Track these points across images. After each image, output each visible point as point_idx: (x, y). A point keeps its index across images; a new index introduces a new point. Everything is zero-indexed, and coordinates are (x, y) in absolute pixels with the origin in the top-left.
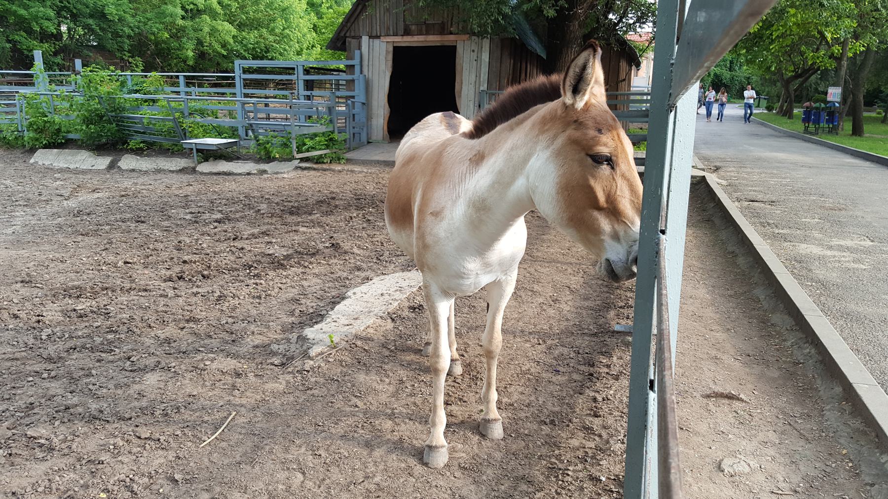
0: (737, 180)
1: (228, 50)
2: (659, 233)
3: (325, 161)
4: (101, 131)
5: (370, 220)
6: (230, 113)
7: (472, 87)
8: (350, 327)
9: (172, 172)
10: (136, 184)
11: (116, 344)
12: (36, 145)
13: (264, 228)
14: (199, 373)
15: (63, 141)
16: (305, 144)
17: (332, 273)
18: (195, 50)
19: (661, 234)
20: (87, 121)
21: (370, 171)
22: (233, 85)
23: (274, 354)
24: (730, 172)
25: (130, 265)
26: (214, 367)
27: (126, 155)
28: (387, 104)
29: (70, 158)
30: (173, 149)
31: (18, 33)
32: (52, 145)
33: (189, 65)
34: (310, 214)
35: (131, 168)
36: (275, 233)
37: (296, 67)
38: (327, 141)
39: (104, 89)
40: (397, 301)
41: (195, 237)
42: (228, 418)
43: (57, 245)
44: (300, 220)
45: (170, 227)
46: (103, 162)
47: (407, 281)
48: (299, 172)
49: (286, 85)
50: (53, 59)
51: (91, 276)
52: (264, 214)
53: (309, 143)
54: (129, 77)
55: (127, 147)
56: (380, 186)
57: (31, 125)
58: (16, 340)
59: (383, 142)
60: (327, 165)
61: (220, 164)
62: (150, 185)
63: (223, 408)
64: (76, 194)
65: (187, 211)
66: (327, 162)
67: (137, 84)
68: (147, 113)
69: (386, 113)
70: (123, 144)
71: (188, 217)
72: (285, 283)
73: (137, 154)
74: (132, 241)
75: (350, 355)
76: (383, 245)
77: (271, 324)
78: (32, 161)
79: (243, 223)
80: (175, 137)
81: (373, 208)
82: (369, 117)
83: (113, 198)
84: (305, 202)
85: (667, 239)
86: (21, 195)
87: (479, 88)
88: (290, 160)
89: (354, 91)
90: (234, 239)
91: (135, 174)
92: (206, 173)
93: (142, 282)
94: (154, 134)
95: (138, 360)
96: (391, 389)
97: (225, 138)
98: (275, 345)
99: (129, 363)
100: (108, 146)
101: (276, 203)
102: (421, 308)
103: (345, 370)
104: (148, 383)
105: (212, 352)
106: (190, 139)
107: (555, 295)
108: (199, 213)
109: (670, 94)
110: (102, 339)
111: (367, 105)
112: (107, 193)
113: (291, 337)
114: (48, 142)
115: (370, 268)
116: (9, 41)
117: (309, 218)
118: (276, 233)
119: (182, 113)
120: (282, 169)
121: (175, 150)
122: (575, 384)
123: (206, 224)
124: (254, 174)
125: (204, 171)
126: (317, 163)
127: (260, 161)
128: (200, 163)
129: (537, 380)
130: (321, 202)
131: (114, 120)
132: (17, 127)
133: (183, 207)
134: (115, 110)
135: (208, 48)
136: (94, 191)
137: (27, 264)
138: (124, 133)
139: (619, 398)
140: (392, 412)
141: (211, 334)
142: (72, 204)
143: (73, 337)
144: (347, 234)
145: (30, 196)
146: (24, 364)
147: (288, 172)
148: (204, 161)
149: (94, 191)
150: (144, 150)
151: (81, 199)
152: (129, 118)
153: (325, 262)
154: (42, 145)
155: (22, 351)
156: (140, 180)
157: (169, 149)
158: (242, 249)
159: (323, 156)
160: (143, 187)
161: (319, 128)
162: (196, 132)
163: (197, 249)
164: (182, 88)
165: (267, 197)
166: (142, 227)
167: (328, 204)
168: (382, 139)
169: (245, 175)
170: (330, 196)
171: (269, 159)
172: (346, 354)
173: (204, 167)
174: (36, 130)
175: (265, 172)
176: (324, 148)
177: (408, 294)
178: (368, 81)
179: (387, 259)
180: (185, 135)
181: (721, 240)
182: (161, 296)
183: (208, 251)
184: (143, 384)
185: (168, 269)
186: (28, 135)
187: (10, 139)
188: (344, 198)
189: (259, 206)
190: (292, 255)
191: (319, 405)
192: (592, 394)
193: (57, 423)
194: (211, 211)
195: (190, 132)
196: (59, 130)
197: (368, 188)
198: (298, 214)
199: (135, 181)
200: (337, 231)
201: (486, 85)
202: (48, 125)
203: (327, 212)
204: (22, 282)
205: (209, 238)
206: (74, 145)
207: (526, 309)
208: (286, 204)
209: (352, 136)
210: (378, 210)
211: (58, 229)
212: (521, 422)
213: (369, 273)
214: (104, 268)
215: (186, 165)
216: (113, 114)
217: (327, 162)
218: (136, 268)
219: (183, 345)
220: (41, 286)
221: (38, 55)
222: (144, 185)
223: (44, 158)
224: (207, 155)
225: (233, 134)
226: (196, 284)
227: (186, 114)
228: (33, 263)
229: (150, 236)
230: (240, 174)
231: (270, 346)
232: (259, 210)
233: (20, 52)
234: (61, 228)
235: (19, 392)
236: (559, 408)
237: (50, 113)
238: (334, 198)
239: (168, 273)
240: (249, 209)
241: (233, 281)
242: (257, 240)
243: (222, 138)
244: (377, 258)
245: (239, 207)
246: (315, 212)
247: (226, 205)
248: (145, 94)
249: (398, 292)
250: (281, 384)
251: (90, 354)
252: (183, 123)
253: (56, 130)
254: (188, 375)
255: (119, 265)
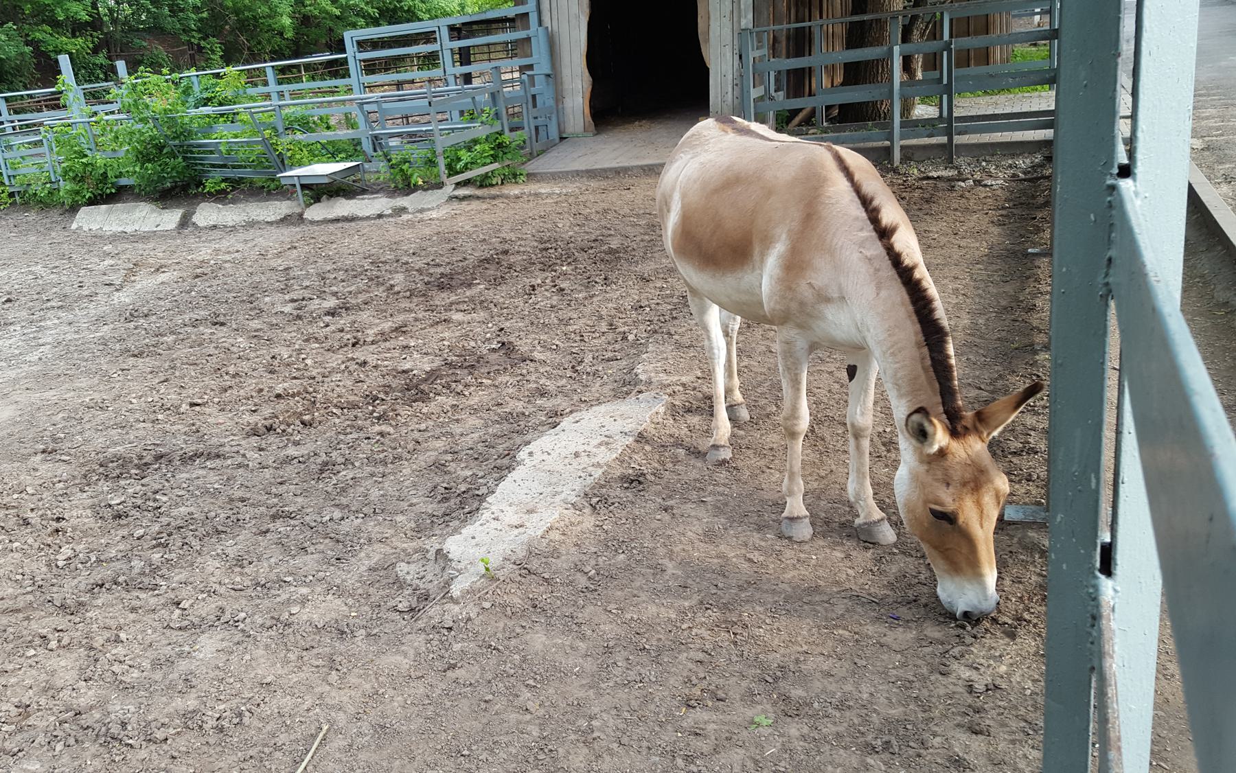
0: (1222, 135)
1: (341, 6)
2: (1098, 574)
3: (494, 182)
4: (163, 170)
5: (563, 290)
6: (347, 117)
7: (727, 22)
8: (521, 530)
9: (270, 223)
10: (217, 251)
11: (164, 571)
12: (77, 201)
13: (400, 319)
14: (281, 631)
15: (113, 191)
16: (459, 159)
17: (499, 404)
18: (294, 13)
19: (1102, 577)
20: (143, 157)
21: (564, 191)
22: (346, 74)
23: (399, 584)
24: (1207, 118)
25: (197, 408)
26: (305, 617)
27: (202, 205)
28: (587, 70)
29: (125, 216)
30: (269, 186)
31: (40, 28)
32: (99, 198)
33: (287, 39)
34: (470, 285)
35: (212, 223)
36: (415, 329)
37: (437, 29)
38: (493, 149)
39: (158, 104)
40: (602, 467)
41: (297, 347)
42: (317, 735)
43: (98, 377)
44: (453, 298)
45: (261, 329)
46: (170, 218)
47: (620, 422)
48: (456, 205)
49: (431, 60)
50: (93, 60)
51: (142, 433)
52: (399, 292)
53: (465, 156)
54: (194, 79)
55: (203, 190)
56: (580, 220)
57: (65, 172)
58: (21, 571)
59: (585, 134)
60: (497, 188)
61: (338, 204)
62: (237, 251)
63: (311, 714)
64: (133, 278)
65: (287, 297)
66: (497, 184)
67: (207, 89)
68: (224, 136)
69: (585, 86)
70: (198, 187)
71: (288, 309)
72: (424, 431)
73: (218, 201)
74: (204, 361)
75: (519, 593)
76: (583, 340)
77: (399, 518)
78: (74, 226)
79: (368, 313)
80: (270, 167)
81: (569, 264)
82: (559, 97)
83: (184, 281)
84: (460, 264)
85: (1118, 588)
86: (54, 290)
87: (739, 22)
88: (440, 186)
89: (532, 56)
90: (354, 345)
91: (216, 234)
92: (318, 221)
93: (214, 441)
94: (240, 167)
95: (192, 605)
96: (590, 665)
97: (342, 160)
98: (403, 564)
99: (178, 612)
100: (177, 190)
101: (417, 270)
102: (641, 479)
103: (510, 623)
104: (201, 656)
105: (305, 584)
106: (291, 169)
107: (888, 430)
108: (303, 299)
109: (1110, 260)
110: (143, 563)
111: (553, 77)
112: (175, 273)
113: (428, 547)
114: (93, 194)
115: (561, 391)
116: (27, 44)
117: (468, 293)
118: (416, 329)
119: (275, 129)
120: (429, 202)
121: (270, 190)
122: (930, 649)
123: (313, 320)
124: (389, 216)
125: (316, 219)
126: (481, 186)
127: (395, 192)
128: (308, 205)
129: (857, 641)
130: (487, 260)
131: (179, 152)
132: (49, 177)
133: (282, 291)
134: (178, 137)
135: (312, 8)
136: (158, 270)
137: (54, 417)
138: (195, 170)
139: (1019, 683)
140: (590, 725)
141: (305, 545)
142: (124, 298)
143: (102, 561)
144: (527, 321)
145: (68, 290)
146: (28, 619)
147: (438, 207)
148: (315, 202)
149: (158, 270)
150: (228, 193)
151: (139, 286)
152: (200, 146)
153: (490, 381)
154: (84, 200)
155: (28, 593)
156: (224, 244)
157: (263, 187)
158: (365, 363)
159: (490, 174)
160: (227, 257)
161: (479, 130)
162: (298, 156)
163: (298, 369)
164: (273, 87)
165: (405, 259)
166: (221, 332)
167: (498, 263)
168: (583, 129)
169: (375, 219)
170: (500, 247)
171: (408, 188)
172: (513, 591)
173: (317, 212)
174: (74, 179)
175: (404, 210)
176: (488, 161)
177: (619, 452)
178: (552, 35)
179: (589, 370)
180: (283, 163)
181: (1202, 276)
182: (240, 466)
183: (314, 373)
184: (195, 658)
185: (254, 411)
186: (66, 186)
187: (42, 195)
188: (522, 249)
189: (393, 278)
190: (440, 370)
191: (464, 704)
192: (967, 674)
193: (59, 747)
194: (321, 295)
195: (290, 158)
196: (105, 175)
197: (560, 225)
198: (451, 288)
199: (217, 246)
200: (510, 316)
201: (750, 16)
202: (90, 170)
203: (495, 280)
204: (44, 452)
205: (317, 345)
206: (129, 194)
207: (833, 467)
208: (431, 271)
209: (533, 132)
210: (576, 268)
211: (101, 347)
212: (828, 747)
213: (560, 402)
214: (160, 417)
215: (289, 212)
216: (177, 142)
217: (497, 184)
218: (207, 413)
219: (262, 570)
220: (68, 458)
221: (64, 61)
222: (229, 252)
223: (92, 219)
224: (318, 192)
225: (356, 150)
226: (292, 438)
227: (281, 130)
228: (61, 415)
229: (232, 348)
230: (368, 218)
231: (395, 567)
232: (392, 286)
233: (45, 54)
234: (106, 345)
235: (13, 680)
236: (901, 709)
237: (91, 150)
238: (506, 252)
239: (253, 419)
240: (378, 285)
241: (349, 430)
242: (387, 344)
243: (337, 162)
244: (573, 367)
245: (361, 283)
246: (478, 281)
247: (343, 281)
248: (221, 104)
249: (603, 448)
250: (405, 655)
251: (124, 594)
252: (277, 145)
253: (102, 174)
254: (264, 637)
255: (182, 410)
